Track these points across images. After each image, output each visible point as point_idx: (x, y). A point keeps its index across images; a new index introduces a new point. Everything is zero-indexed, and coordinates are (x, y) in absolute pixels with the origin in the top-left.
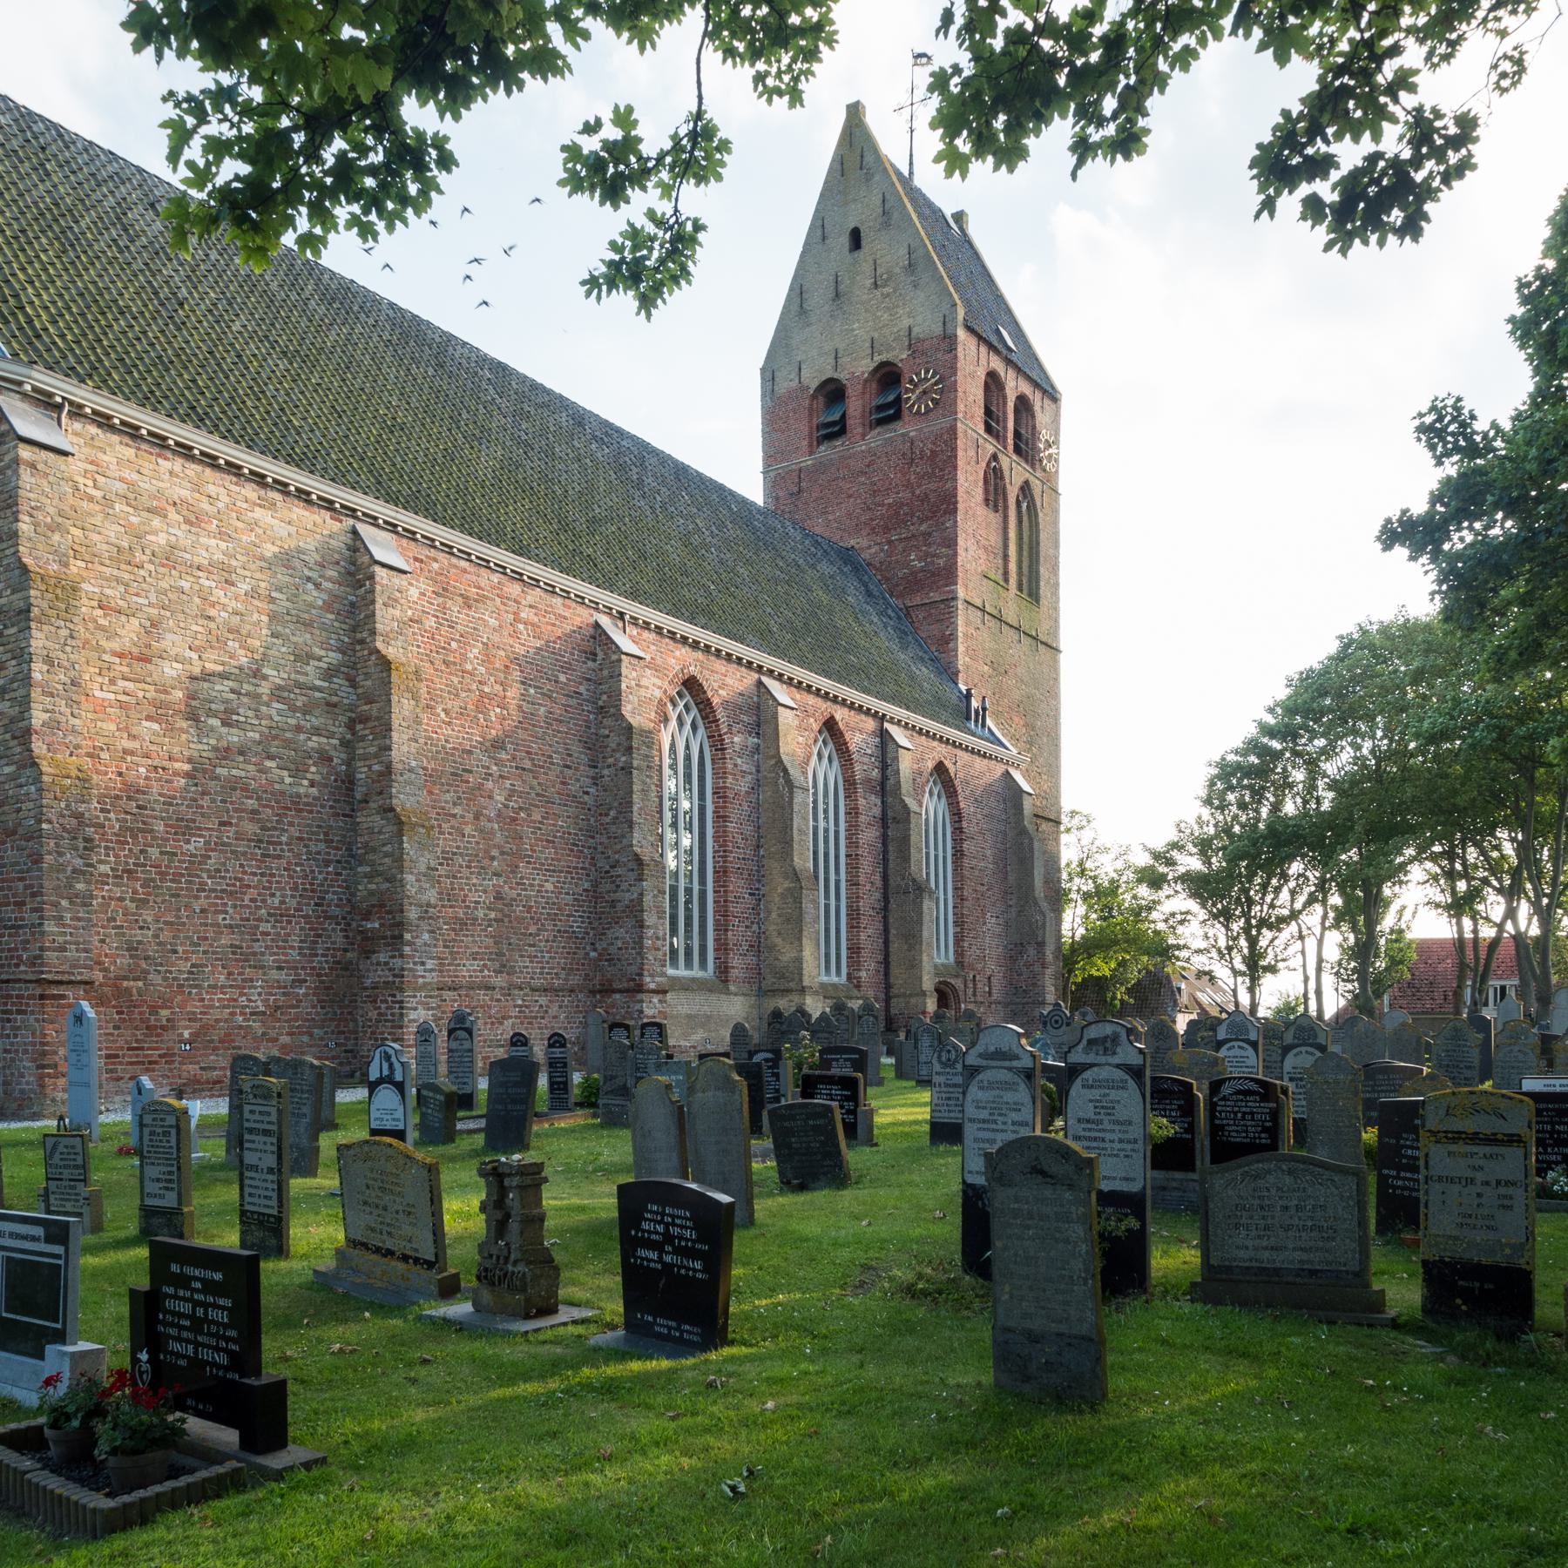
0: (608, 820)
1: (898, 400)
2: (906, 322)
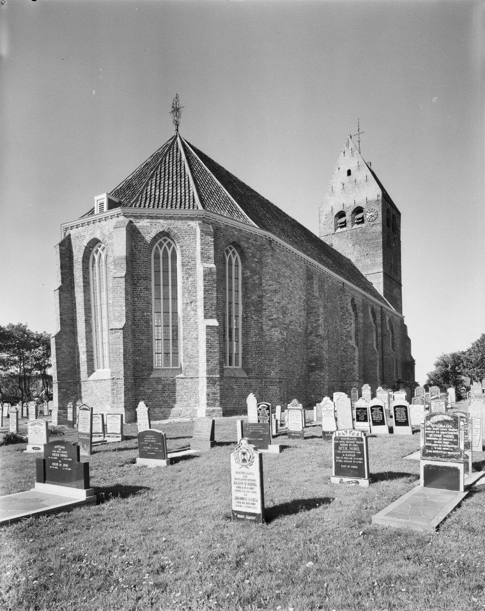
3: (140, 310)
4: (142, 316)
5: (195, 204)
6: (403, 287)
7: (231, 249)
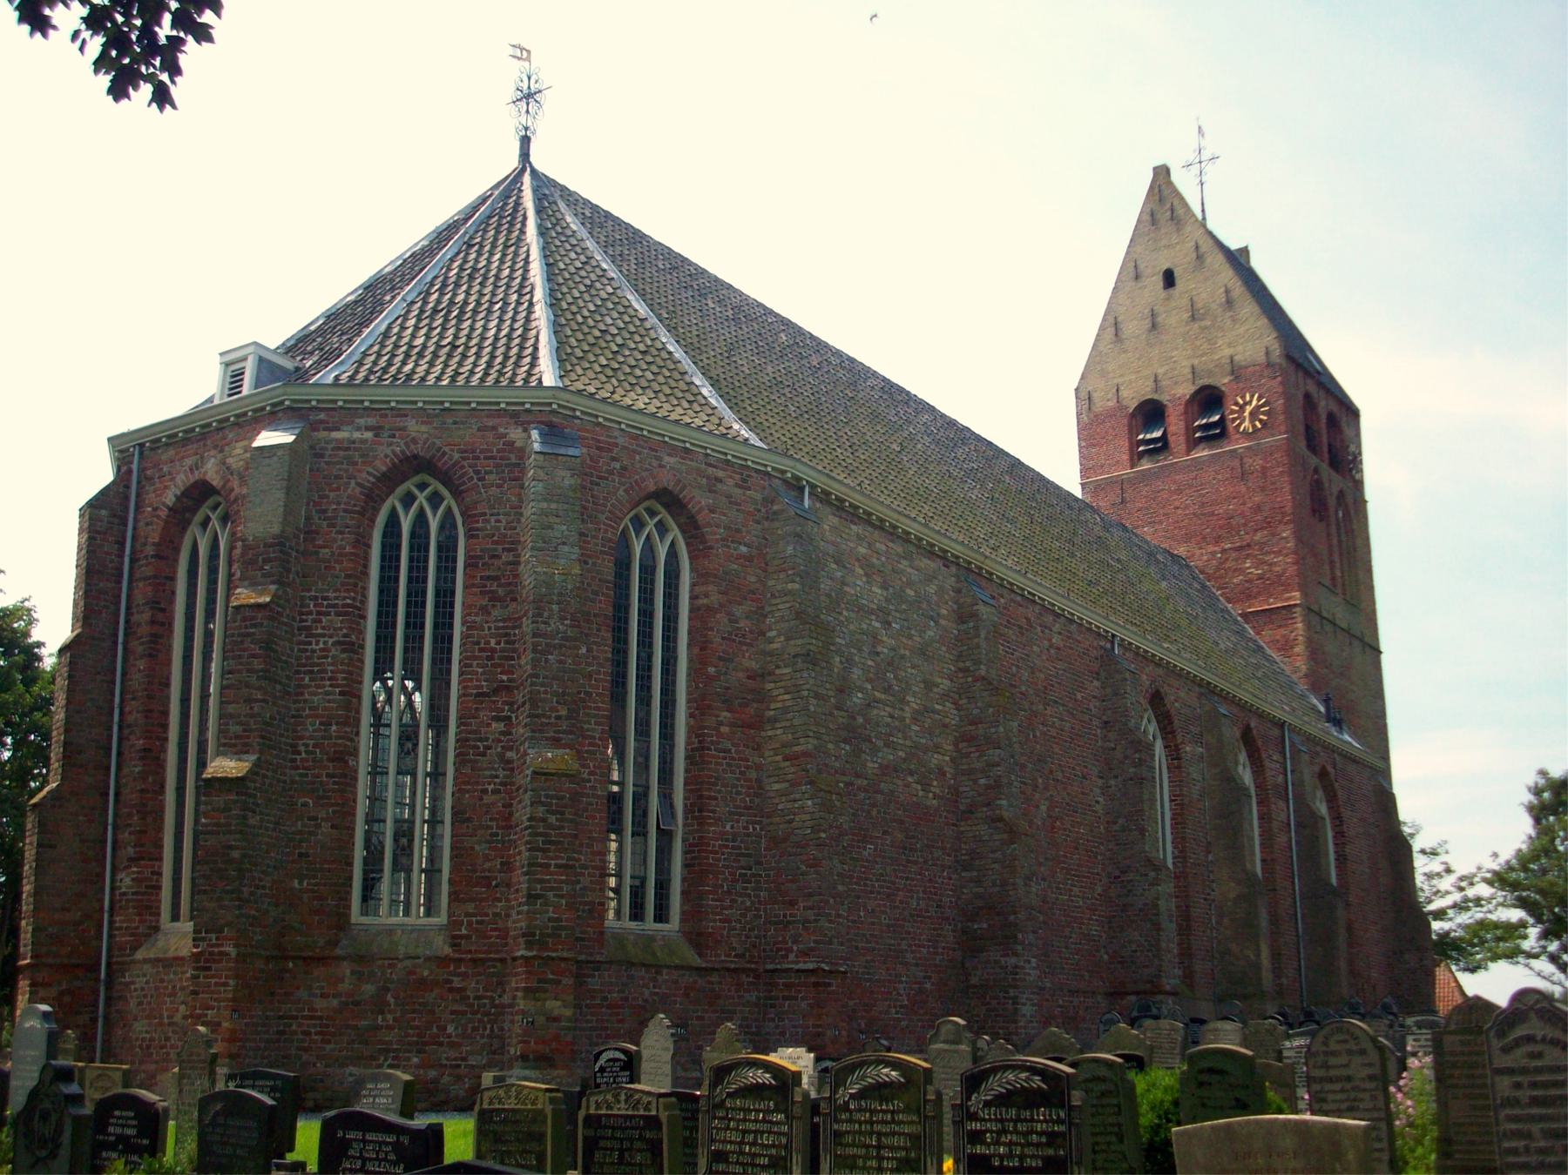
0: (1116, 827)
1: (1222, 419)
2: (1227, 352)
3: (317, 716)
4: (323, 738)
5: (536, 370)
6: (1383, 657)
7: (652, 513)
